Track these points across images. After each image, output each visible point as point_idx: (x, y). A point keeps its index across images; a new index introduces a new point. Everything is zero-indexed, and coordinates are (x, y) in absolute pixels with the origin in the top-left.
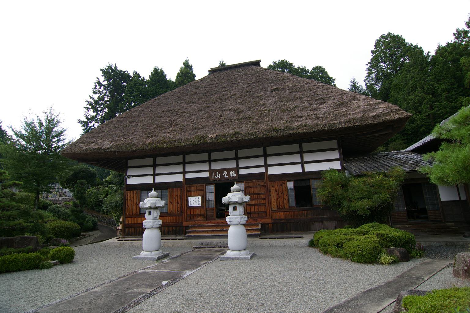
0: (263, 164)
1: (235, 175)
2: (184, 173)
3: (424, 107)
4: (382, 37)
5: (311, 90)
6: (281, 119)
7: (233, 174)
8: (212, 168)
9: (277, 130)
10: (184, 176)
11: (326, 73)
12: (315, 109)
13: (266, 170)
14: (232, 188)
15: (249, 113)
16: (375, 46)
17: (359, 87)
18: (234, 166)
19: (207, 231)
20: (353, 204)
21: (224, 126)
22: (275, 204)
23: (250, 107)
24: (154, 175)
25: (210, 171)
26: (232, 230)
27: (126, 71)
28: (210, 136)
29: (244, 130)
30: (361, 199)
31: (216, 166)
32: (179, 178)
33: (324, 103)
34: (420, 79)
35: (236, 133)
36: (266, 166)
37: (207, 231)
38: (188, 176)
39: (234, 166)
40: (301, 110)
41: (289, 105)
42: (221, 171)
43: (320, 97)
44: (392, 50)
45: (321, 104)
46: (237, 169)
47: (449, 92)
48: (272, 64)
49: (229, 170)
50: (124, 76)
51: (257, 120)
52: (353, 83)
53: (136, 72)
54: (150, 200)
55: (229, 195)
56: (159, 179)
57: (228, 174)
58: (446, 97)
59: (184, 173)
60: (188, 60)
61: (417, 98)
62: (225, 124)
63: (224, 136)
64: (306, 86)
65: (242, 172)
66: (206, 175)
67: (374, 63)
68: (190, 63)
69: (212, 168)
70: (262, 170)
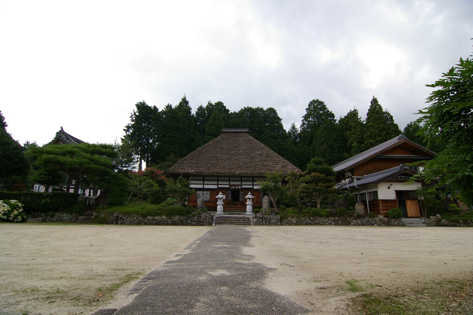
0: (252, 184)
1: (240, 188)
2: (218, 185)
3: (327, 155)
4: (313, 100)
5: (273, 157)
6: (262, 169)
7: (240, 187)
8: (231, 184)
9: (261, 174)
10: (218, 186)
11: (277, 114)
12: (274, 167)
13: (253, 187)
14: (248, 194)
15: (250, 165)
16: (309, 106)
17: (296, 129)
18: (240, 184)
19: (229, 209)
20: (284, 201)
21: (241, 169)
22: (256, 200)
23: (250, 161)
24: (203, 184)
25: (229, 185)
26: (248, 207)
27: (151, 107)
28: (237, 173)
29: (250, 171)
30: (286, 200)
31: (232, 183)
32: (215, 187)
33: (278, 165)
34: (327, 138)
35: (247, 173)
36: (253, 185)
37: (229, 209)
38: (219, 186)
39: (240, 184)
40: (270, 167)
41: (266, 164)
42: (235, 185)
43: (277, 162)
44: (317, 111)
45: (277, 165)
46: (241, 185)
47: (339, 149)
48: (243, 109)
49: (238, 185)
50: (147, 107)
51: (254, 168)
52: (293, 126)
53: (156, 107)
54: (249, 196)
55: (218, 196)
56: (206, 187)
57: (238, 187)
58: (337, 151)
59: (218, 185)
60: (186, 97)
61: (324, 149)
62: (241, 168)
63: (242, 173)
64: (272, 154)
65: (243, 187)
66: (228, 186)
67: (306, 117)
68: (187, 99)
69: (231, 184)
70: (251, 187)
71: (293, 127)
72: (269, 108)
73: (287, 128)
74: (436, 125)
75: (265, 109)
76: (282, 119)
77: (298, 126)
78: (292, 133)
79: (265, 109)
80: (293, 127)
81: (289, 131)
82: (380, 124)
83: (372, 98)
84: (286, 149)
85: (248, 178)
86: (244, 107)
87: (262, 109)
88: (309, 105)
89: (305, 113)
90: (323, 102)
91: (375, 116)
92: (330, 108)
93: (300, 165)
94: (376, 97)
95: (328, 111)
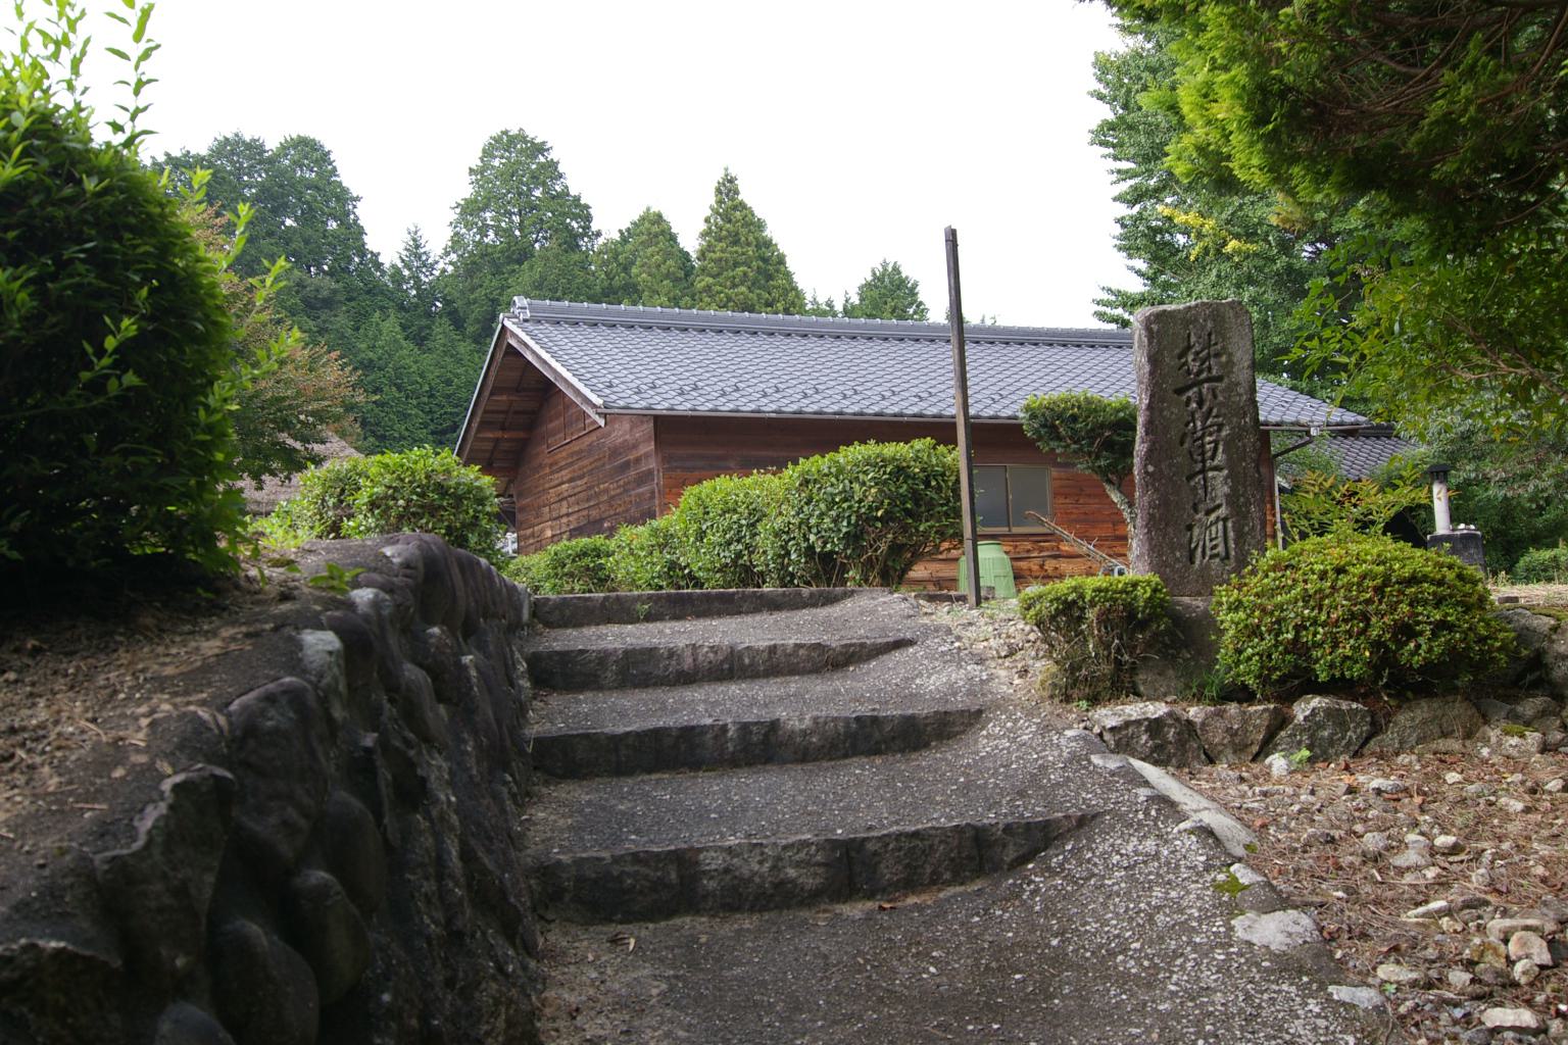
52: (414, 240)
67: (469, 210)
71: (415, 248)
72: (294, 136)
73: (385, 243)
74: (1383, 188)
75: (272, 144)
76: (358, 199)
77: (437, 241)
78: (406, 273)
79: (272, 144)
80: (415, 248)
81: (394, 266)
82: (734, 286)
83: (719, 176)
84: (371, 361)
85: (833, 640)
86: (167, 154)
87: (255, 148)
88: (487, 153)
89: (465, 190)
90: (544, 143)
91: (722, 251)
92: (577, 180)
93: (433, 433)
94: (733, 172)
95: (565, 193)
